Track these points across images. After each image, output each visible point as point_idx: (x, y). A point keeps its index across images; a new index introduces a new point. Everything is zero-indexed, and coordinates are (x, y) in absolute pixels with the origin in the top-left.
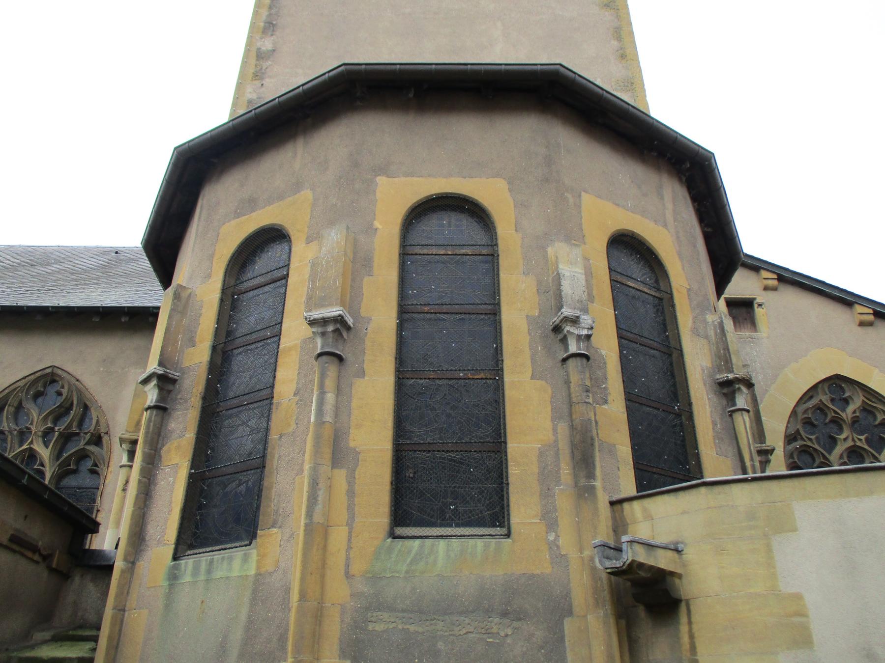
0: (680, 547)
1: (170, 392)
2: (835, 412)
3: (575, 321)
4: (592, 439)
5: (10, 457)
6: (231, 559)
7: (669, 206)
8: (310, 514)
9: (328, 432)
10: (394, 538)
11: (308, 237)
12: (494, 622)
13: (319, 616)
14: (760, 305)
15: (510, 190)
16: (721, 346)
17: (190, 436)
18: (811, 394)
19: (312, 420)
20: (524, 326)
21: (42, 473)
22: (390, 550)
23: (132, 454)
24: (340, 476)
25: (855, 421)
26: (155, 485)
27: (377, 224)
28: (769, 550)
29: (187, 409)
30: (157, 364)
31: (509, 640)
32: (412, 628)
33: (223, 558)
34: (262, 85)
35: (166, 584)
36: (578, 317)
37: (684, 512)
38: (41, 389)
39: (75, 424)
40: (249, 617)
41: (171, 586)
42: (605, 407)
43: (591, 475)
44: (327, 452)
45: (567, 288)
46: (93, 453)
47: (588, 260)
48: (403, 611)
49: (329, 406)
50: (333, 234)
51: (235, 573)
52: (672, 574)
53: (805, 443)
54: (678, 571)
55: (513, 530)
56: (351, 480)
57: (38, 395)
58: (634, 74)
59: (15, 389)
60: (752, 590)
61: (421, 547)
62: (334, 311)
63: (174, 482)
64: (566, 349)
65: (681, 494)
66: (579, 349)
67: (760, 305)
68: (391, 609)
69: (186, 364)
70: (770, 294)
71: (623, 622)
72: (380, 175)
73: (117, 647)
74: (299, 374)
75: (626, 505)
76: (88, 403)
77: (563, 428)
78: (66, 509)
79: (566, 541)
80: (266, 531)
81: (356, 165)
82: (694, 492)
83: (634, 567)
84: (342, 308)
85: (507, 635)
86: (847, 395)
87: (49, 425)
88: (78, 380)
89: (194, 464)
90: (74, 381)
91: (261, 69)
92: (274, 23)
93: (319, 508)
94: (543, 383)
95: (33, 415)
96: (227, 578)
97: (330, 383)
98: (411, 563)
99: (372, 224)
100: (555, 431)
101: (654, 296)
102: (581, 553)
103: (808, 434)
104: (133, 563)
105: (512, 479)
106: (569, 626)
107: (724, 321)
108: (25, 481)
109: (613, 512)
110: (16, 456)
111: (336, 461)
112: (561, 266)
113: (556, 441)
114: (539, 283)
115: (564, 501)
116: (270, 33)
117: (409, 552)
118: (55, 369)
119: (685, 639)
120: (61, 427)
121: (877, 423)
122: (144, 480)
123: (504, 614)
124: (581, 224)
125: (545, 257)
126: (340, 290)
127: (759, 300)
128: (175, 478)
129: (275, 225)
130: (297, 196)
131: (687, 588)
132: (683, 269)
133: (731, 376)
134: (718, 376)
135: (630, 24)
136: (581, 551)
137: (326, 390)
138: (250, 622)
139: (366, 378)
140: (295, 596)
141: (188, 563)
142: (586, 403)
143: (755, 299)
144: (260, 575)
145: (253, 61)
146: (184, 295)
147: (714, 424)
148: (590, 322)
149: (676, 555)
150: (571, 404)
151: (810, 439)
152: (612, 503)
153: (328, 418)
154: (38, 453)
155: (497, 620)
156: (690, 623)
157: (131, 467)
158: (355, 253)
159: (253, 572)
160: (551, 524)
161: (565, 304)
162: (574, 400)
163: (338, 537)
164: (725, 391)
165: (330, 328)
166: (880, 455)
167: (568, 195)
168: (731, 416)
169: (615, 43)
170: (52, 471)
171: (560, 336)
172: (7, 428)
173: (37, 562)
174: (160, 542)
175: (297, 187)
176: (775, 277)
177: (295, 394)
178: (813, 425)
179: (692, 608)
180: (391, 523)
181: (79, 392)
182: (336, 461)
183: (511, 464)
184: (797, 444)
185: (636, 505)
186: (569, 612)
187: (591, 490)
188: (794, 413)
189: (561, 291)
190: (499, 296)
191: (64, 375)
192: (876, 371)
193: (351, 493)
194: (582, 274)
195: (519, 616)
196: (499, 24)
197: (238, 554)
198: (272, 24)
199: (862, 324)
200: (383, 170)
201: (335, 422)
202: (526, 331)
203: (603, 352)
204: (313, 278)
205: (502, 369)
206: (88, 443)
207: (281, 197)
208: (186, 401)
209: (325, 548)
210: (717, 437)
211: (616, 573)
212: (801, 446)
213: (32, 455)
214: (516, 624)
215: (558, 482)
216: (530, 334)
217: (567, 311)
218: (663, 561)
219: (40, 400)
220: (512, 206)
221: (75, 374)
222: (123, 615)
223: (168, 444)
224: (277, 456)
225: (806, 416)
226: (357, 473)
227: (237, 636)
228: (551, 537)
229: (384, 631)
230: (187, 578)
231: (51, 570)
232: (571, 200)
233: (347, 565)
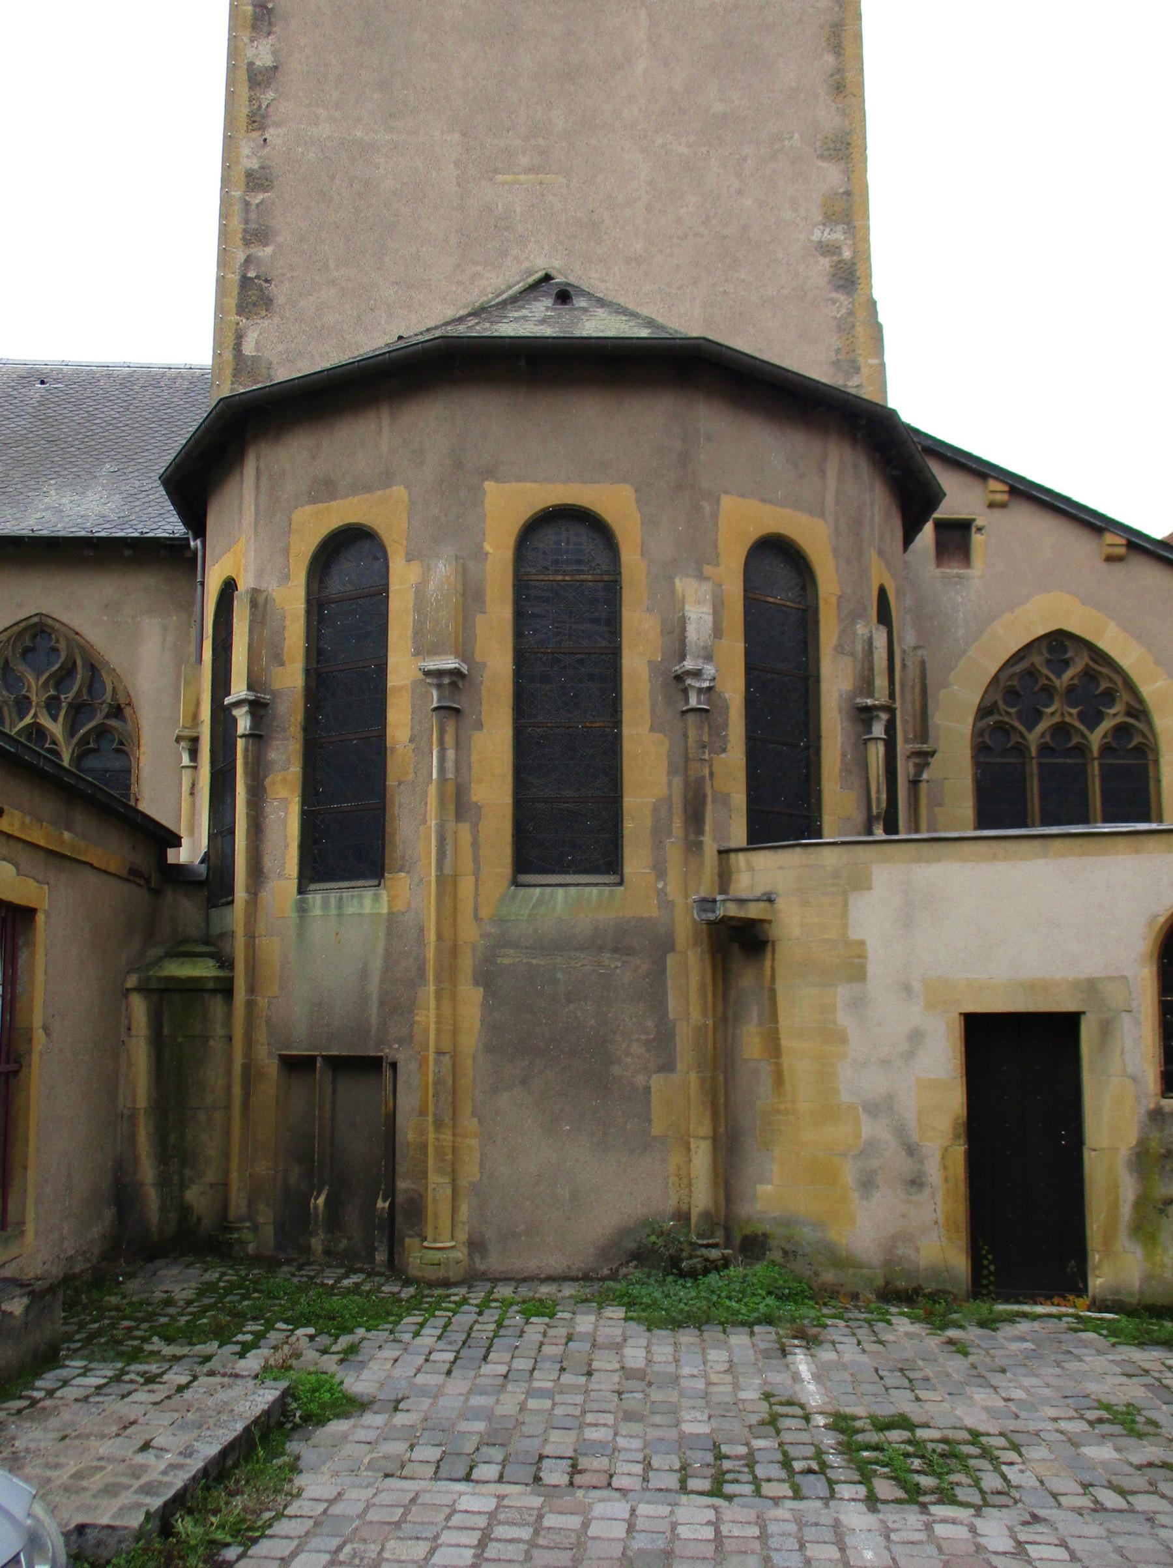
0: (773, 896)
1: (262, 717)
2: (1048, 678)
3: (697, 674)
5: (13, 734)
6: (361, 897)
7: (832, 482)
8: (440, 866)
9: (451, 789)
10: (517, 886)
11: (407, 554)
12: (606, 958)
13: (454, 952)
14: (979, 529)
15: (638, 501)
16: (866, 665)
17: (295, 770)
18: (1022, 655)
19: (435, 776)
20: (645, 674)
21: (57, 754)
22: (513, 897)
23: (194, 754)
24: (465, 830)
25: (1071, 689)
26: (265, 818)
27: (488, 547)
28: (845, 904)
29: (288, 740)
30: (245, 687)
31: (618, 971)
32: (534, 962)
33: (353, 896)
34: (265, 140)
35: (295, 915)
36: (700, 670)
37: (780, 868)
38: (29, 643)
39: (85, 691)
40: (386, 950)
41: (302, 918)
42: (723, 755)
43: (700, 831)
44: (451, 807)
46: (116, 729)
47: (720, 586)
48: (527, 948)
49: (450, 764)
50: (441, 565)
51: (367, 911)
52: (761, 921)
53: (1001, 718)
54: (768, 917)
55: (625, 879)
57: (26, 651)
58: (854, 126)
60: (826, 936)
61: (542, 894)
62: (449, 663)
64: (687, 701)
65: (780, 851)
66: (699, 702)
67: (979, 529)
68: (516, 946)
69: (276, 686)
70: (997, 513)
71: (719, 956)
72: (487, 479)
73: (254, 967)
74: (412, 718)
75: (732, 856)
76: (96, 664)
77: (678, 781)
78: (139, 820)
79: (673, 888)
80: (394, 875)
81: (459, 465)
82: (790, 851)
83: (725, 921)
84: (457, 660)
85: (617, 967)
86: (1069, 655)
87: (52, 692)
88: (77, 634)
89: (304, 801)
90: (72, 635)
91: (260, 107)
92: (270, 5)
93: (448, 862)
94: (661, 736)
95: (28, 680)
96: (360, 914)
97: (449, 739)
98: (533, 908)
99: (482, 547)
100: (670, 785)
101: (798, 609)
102: (686, 899)
104: (256, 894)
105: (626, 832)
106: (671, 959)
107: (874, 636)
109: (720, 860)
110: (19, 733)
111: (459, 816)
112: (687, 607)
113: (670, 796)
114: (664, 622)
115: (674, 853)
116: (265, 29)
117: (531, 899)
118: (43, 617)
119: (768, 972)
120: (67, 698)
121: (1098, 692)
122: (252, 812)
123: (615, 950)
124: (716, 540)
125: (673, 591)
126: (453, 636)
127: (979, 522)
128: (286, 814)
129: (364, 525)
130: (388, 491)
131: (775, 932)
133: (869, 702)
134: (858, 700)
135: (858, 16)
136: (686, 897)
137: (447, 746)
138: (388, 955)
139: (485, 730)
140: (432, 936)
141: (316, 899)
142: (701, 759)
143: (974, 520)
144: (393, 913)
145: (244, 91)
146: (261, 600)
147: (844, 755)
148: (713, 672)
149: (767, 904)
150: (687, 760)
151: (1008, 713)
152: (720, 852)
153: (450, 775)
154: (49, 730)
155: (608, 955)
156: (773, 960)
157: (195, 768)
158: (465, 583)
159: (385, 911)
160: (661, 874)
161: (688, 652)
162: (690, 756)
163: (466, 885)
164: (863, 716)
165: (446, 681)
166: (1092, 733)
167: (704, 504)
168: (865, 744)
169: (830, 58)
170: (70, 751)
171: (681, 686)
173: (140, 885)
174: (280, 876)
175: (387, 479)
176: (1006, 488)
177: (411, 741)
178: (1018, 694)
179: (776, 948)
180: (513, 873)
181: (83, 650)
182: (459, 816)
183: (626, 818)
184: (991, 720)
185: (741, 856)
186: (672, 948)
187: (699, 845)
188: (995, 679)
189: (685, 637)
190: (621, 638)
191: (57, 626)
192: (1113, 624)
193: (475, 845)
194: (709, 614)
195: (630, 952)
197: (368, 895)
198: (266, 8)
199: (1110, 559)
200: (491, 473)
201: (456, 777)
202: (647, 678)
203: (727, 696)
204: (419, 608)
205: (621, 721)
206: (107, 716)
207: (368, 488)
208: (284, 730)
209: (455, 897)
210: (846, 770)
211: (710, 923)
212: (995, 723)
213: (37, 732)
214: (624, 958)
215: (670, 835)
216: (650, 681)
217: (689, 664)
218: (754, 911)
219: (29, 655)
220: (639, 521)
221: (72, 625)
222: (254, 941)
223: (272, 776)
224: (397, 803)
225: (1009, 683)
226: (480, 826)
227: (376, 965)
228: (660, 886)
229: (511, 965)
230: (317, 912)
231: (150, 889)
233: (476, 909)
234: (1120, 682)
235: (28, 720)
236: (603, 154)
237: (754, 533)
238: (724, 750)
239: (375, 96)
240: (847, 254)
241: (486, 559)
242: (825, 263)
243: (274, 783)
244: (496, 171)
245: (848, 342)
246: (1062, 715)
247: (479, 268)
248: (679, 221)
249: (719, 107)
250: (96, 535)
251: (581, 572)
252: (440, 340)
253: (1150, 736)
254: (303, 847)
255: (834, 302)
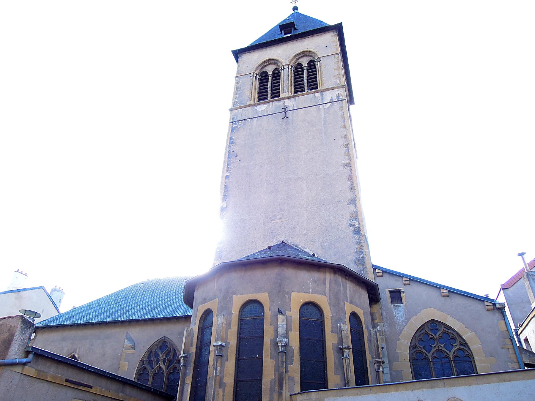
3: (281, 341)
4: (283, 378)
9: (218, 378)
20: (269, 342)
24: (221, 391)
27: (233, 312)
45: (280, 330)
56: (224, 392)
59: (154, 345)
63: (188, 388)
67: (403, 292)
77: (277, 374)
103: (420, 345)
108: (152, 391)
111: (220, 387)
132: (330, 309)
137: (218, 366)
142: (282, 367)
147: (335, 363)
152: (290, 395)
169: (349, 182)
172: (153, 359)
181: (172, 345)
193: (223, 395)
196: (305, 182)
199: (444, 296)
210: (336, 369)
221: (171, 339)
232: (287, 297)
234: (456, 335)
235: (158, 365)
236: (296, 212)
237: (302, 301)
238: (292, 364)
239: (247, 209)
240: (357, 225)
241: (232, 315)
242: (351, 228)
243: (187, 379)
244: (272, 220)
245: (359, 247)
246: (438, 347)
247: (268, 242)
248: (315, 224)
249: (323, 198)
250: (130, 319)
251: (256, 316)
252: (221, 264)
253: (471, 353)
254: (190, 397)
255: (354, 237)
